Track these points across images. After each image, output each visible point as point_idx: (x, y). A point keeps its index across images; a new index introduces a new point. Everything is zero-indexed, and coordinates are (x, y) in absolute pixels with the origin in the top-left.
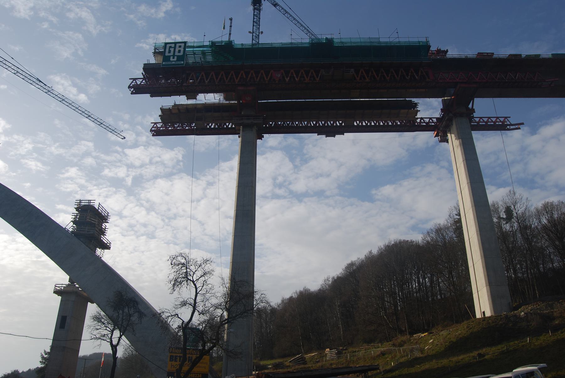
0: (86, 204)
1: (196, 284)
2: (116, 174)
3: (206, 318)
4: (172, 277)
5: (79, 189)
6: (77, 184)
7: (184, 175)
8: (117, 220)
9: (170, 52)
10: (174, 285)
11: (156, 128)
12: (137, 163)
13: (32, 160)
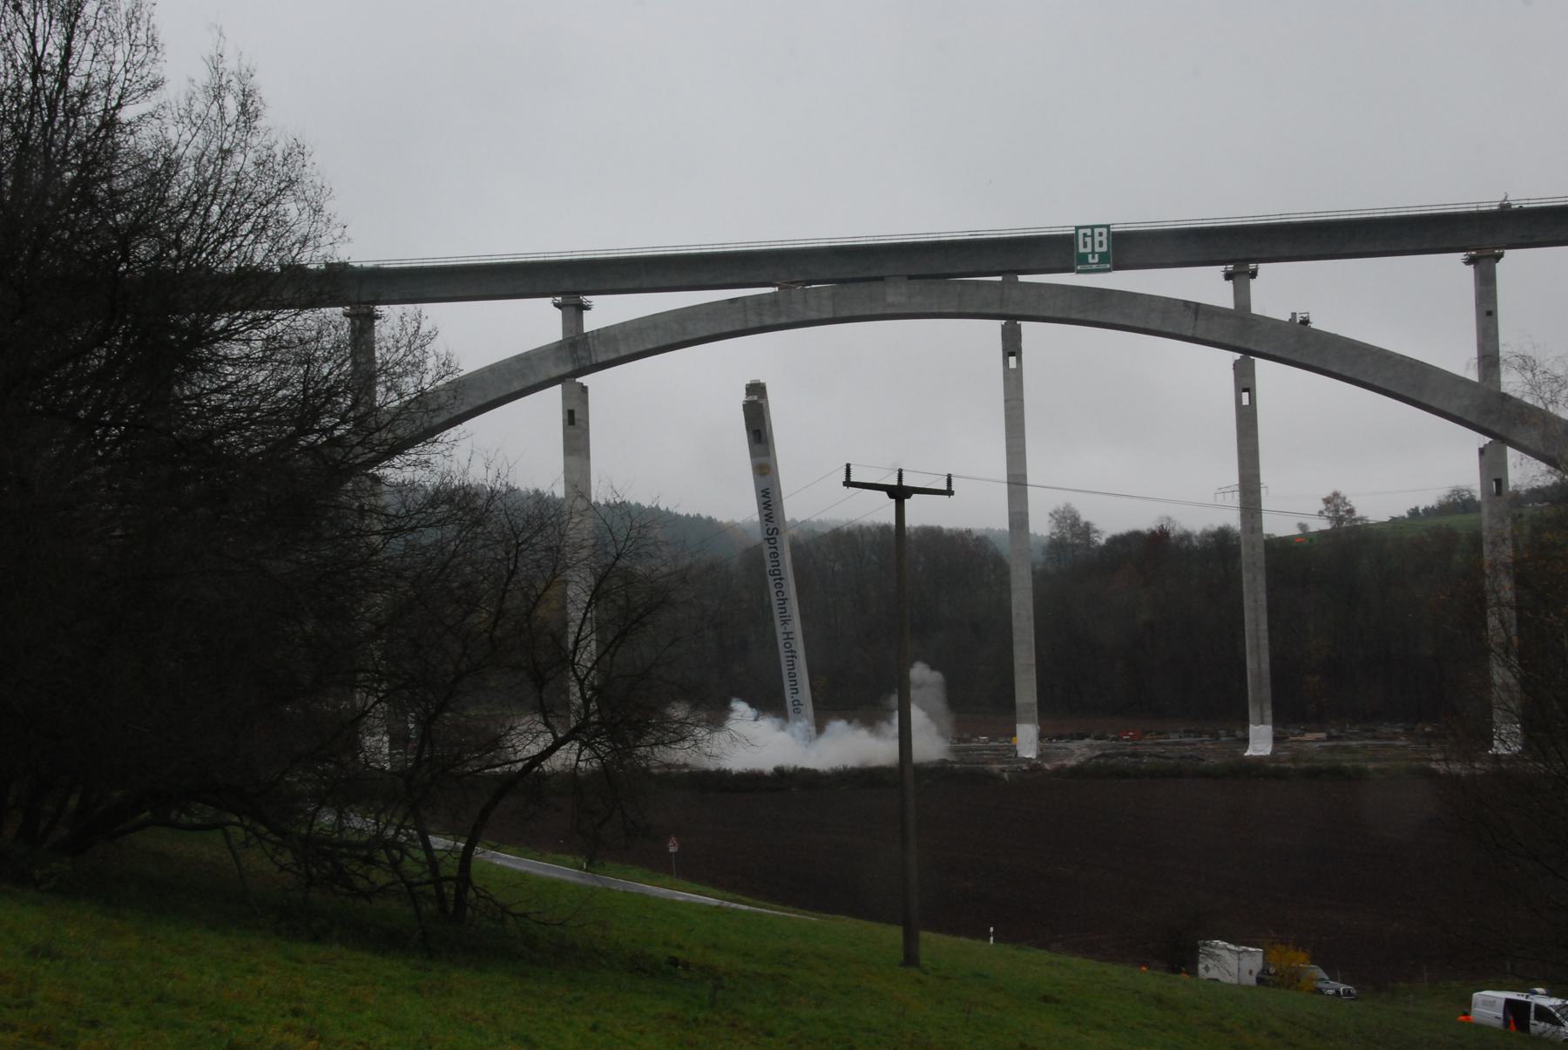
9: (1085, 245)
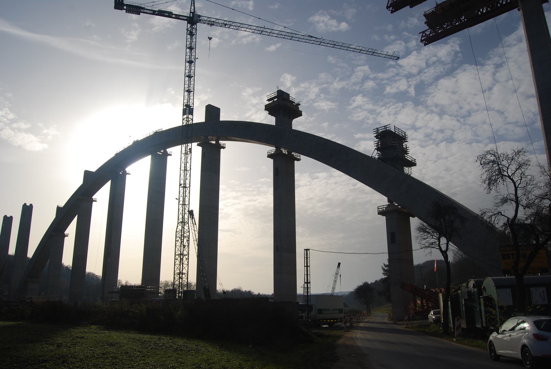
0: (383, 130)
1: (513, 179)
2: (398, 88)
3: (533, 211)
4: (484, 177)
5: (370, 114)
6: (366, 110)
7: (467, 66)
8: (413, 133)
10: (489, 184)
11: (425, 36)
12: (415, 71)
13: (322, 101)
